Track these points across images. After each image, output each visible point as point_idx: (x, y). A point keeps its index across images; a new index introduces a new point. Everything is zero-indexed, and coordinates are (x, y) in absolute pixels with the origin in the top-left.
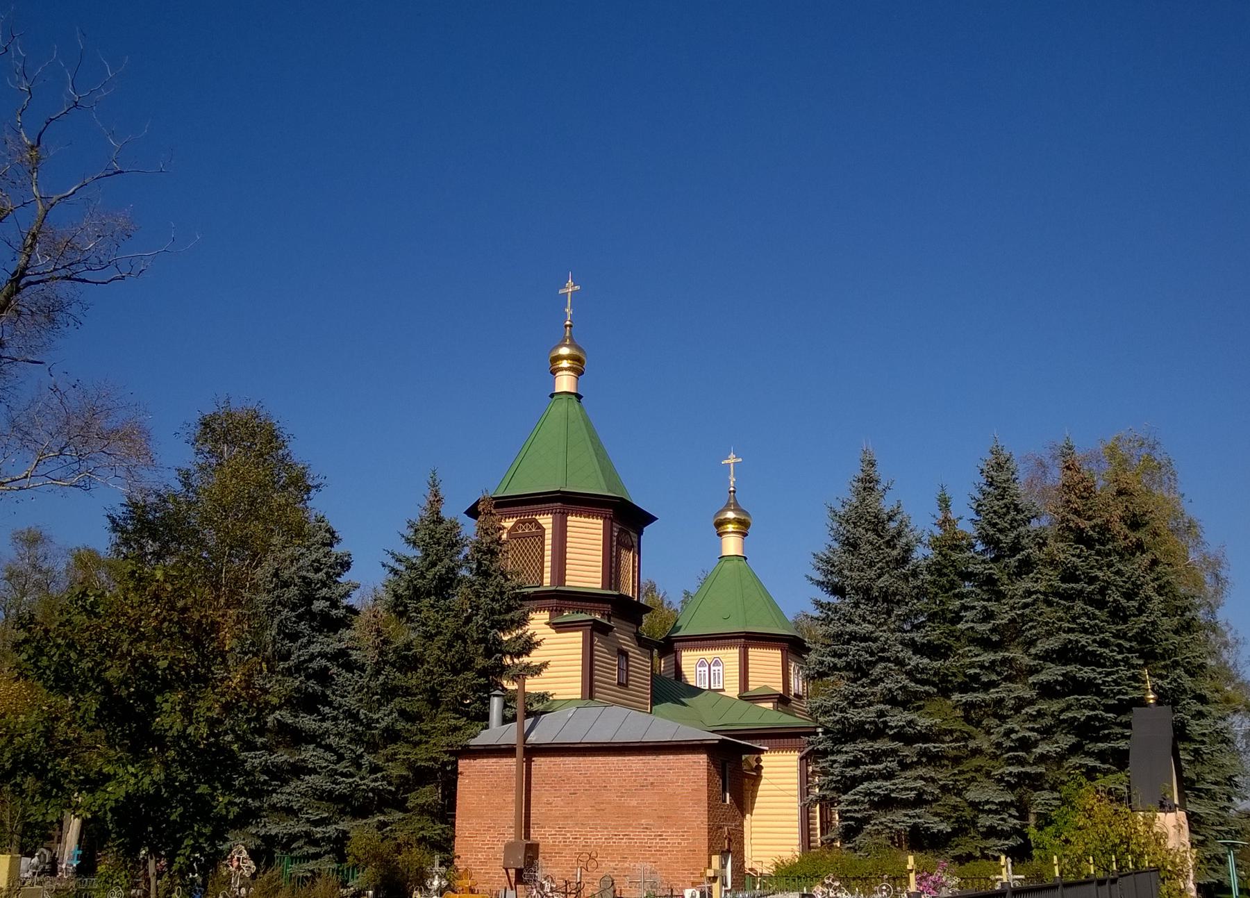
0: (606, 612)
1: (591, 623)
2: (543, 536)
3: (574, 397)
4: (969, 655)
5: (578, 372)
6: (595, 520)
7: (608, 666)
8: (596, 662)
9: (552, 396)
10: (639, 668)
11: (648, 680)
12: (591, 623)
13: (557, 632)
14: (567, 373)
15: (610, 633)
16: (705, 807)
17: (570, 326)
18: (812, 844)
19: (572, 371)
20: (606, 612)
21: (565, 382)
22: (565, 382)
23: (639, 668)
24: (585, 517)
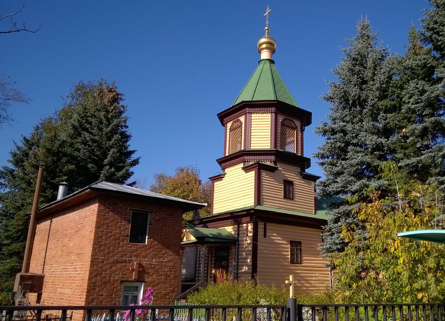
0: (272, 160)
1: (257, 165)
2: (241, 126)
3: (268, 61)
4: (435, 89)
5: (272, 51)
6: (267, 115)
7: (274, 188)
8: (296, 190)
9: (259, 62)
10: (303, 190)
11: (282, 191)
12: (257, 165)
13: (246, 172)
14: (265, 50)
15: (275, 171)
16: (88, 261)
17: (268, 29)
18: (215, 309)
19: (267, 49)
20: (272, 160)
21: (265, 55)
22: (265, 55)
23: (303, 190)
24: (261, 114)
